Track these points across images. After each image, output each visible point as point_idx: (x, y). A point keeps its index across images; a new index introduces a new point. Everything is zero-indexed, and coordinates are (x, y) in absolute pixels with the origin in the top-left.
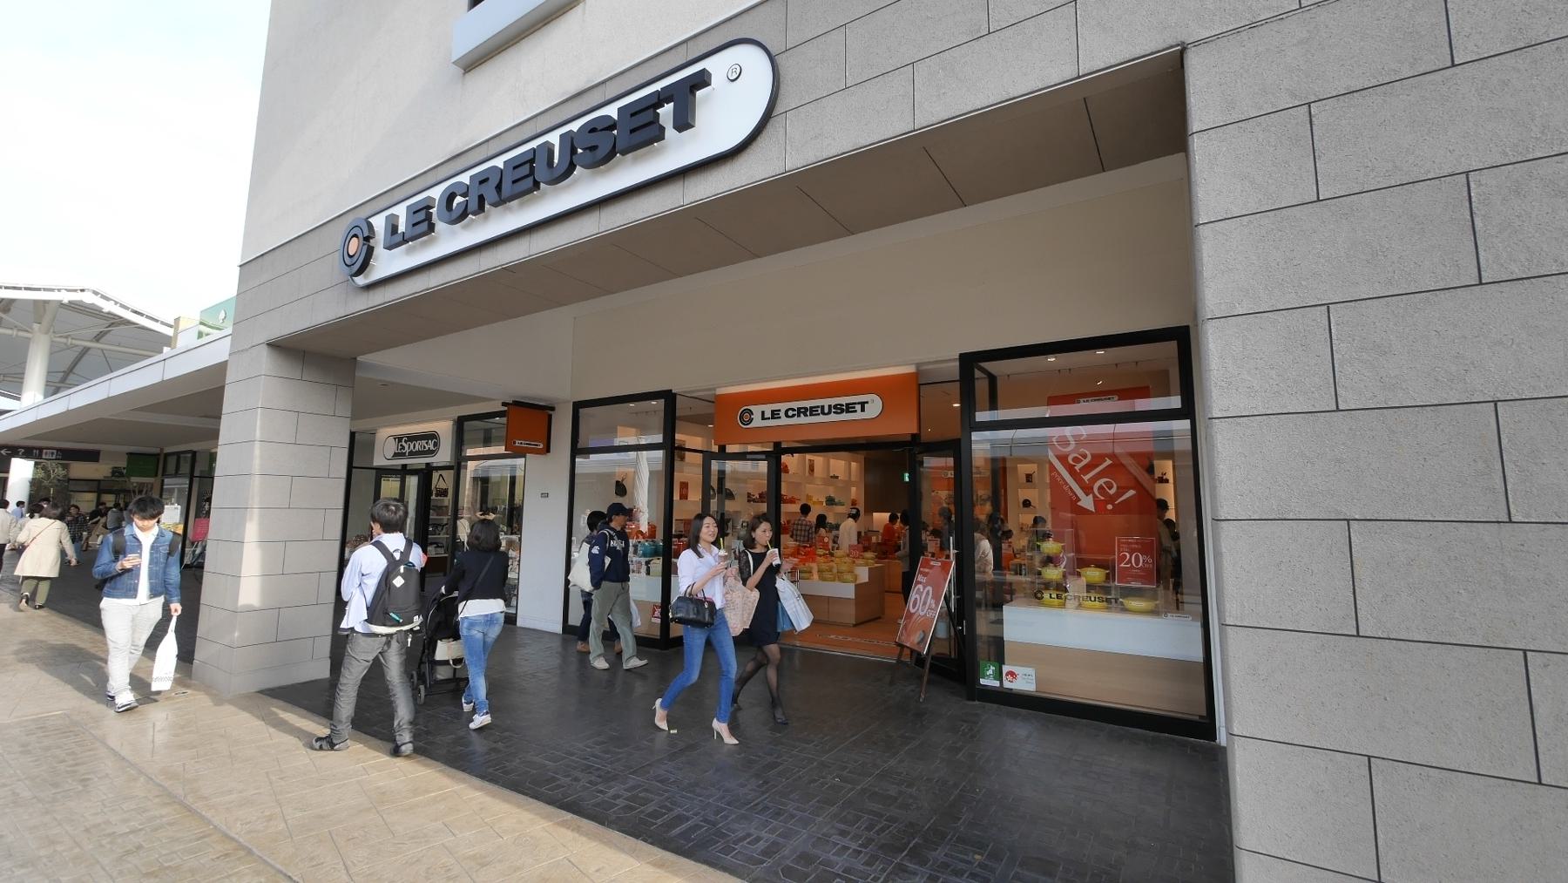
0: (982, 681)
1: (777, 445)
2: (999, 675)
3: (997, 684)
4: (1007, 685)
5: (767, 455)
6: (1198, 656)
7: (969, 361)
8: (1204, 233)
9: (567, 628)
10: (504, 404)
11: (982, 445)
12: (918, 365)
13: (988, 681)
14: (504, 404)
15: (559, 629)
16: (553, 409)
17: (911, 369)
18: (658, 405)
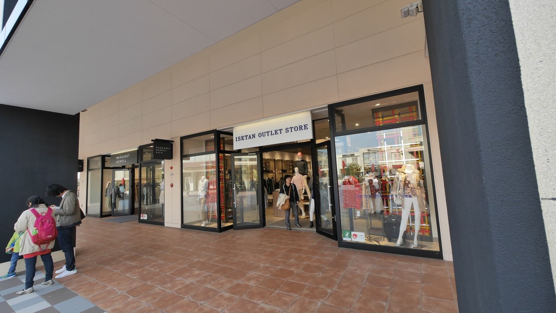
0: (344, 239)
5: (257, 153)
9: (184, 226)
10: (152, 140)
11: (339, 142)
13: (346, 239)
14: (152, 140)
15: (179, 226)
16: (173, 141)
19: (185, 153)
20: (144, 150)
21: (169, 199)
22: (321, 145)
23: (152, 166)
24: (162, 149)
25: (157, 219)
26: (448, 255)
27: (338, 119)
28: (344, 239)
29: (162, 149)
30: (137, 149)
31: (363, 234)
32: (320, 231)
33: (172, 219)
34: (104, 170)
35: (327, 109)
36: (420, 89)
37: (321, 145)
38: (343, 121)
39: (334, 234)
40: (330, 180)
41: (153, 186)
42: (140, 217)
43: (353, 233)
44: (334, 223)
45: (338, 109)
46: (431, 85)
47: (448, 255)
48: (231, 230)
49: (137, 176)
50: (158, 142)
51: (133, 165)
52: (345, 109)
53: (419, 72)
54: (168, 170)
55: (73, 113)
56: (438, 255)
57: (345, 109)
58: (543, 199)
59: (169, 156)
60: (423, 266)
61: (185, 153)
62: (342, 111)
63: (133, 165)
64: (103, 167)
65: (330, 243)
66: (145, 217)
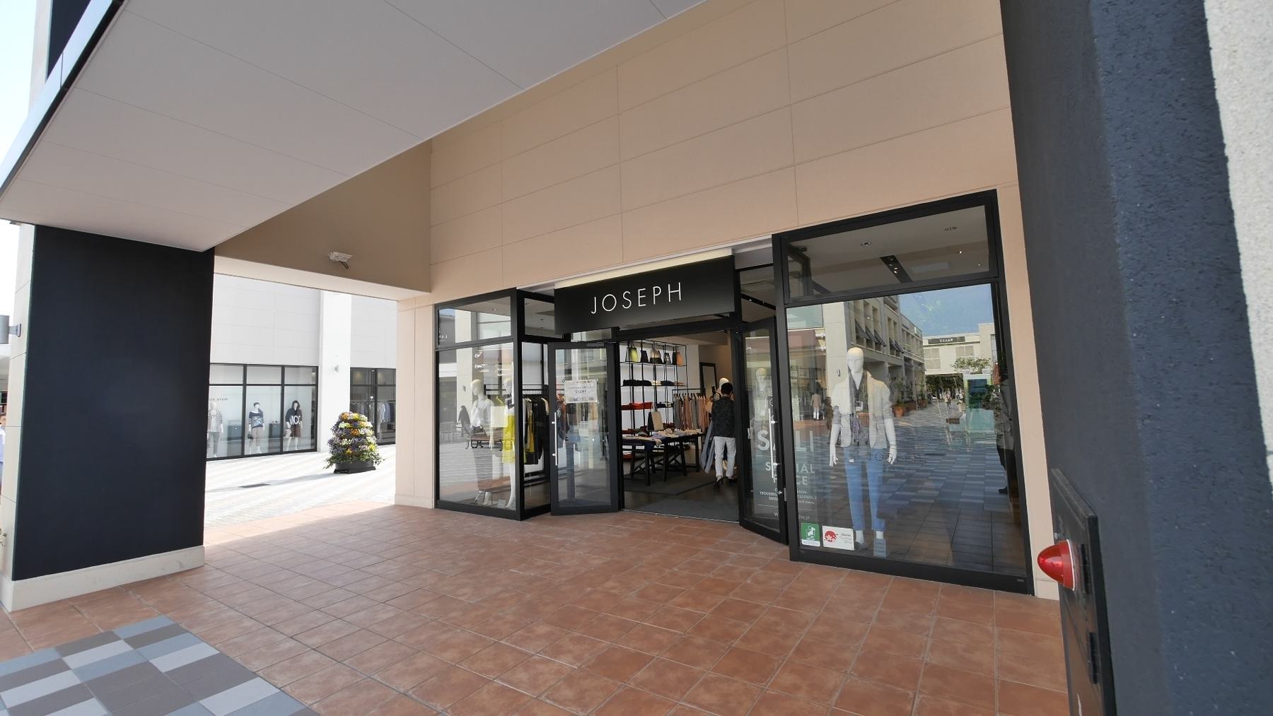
0: (804, 542)
3: (817, 544)
4: (827, 544)
5: (604, 343)
7: (786, 244)
11: (796, 320)
15: (429, 503)
17: (728, 253)
28: (804, 542)
35: (771, 245)
36: (988, 200)
37: (756, 326)
38: (806, 272)
39: (783, 530)
43: (826, 529)
44: (783, 505)
48: (548, 516)
52: (814, 246)
57: (814, 246)
62: (805, 249)
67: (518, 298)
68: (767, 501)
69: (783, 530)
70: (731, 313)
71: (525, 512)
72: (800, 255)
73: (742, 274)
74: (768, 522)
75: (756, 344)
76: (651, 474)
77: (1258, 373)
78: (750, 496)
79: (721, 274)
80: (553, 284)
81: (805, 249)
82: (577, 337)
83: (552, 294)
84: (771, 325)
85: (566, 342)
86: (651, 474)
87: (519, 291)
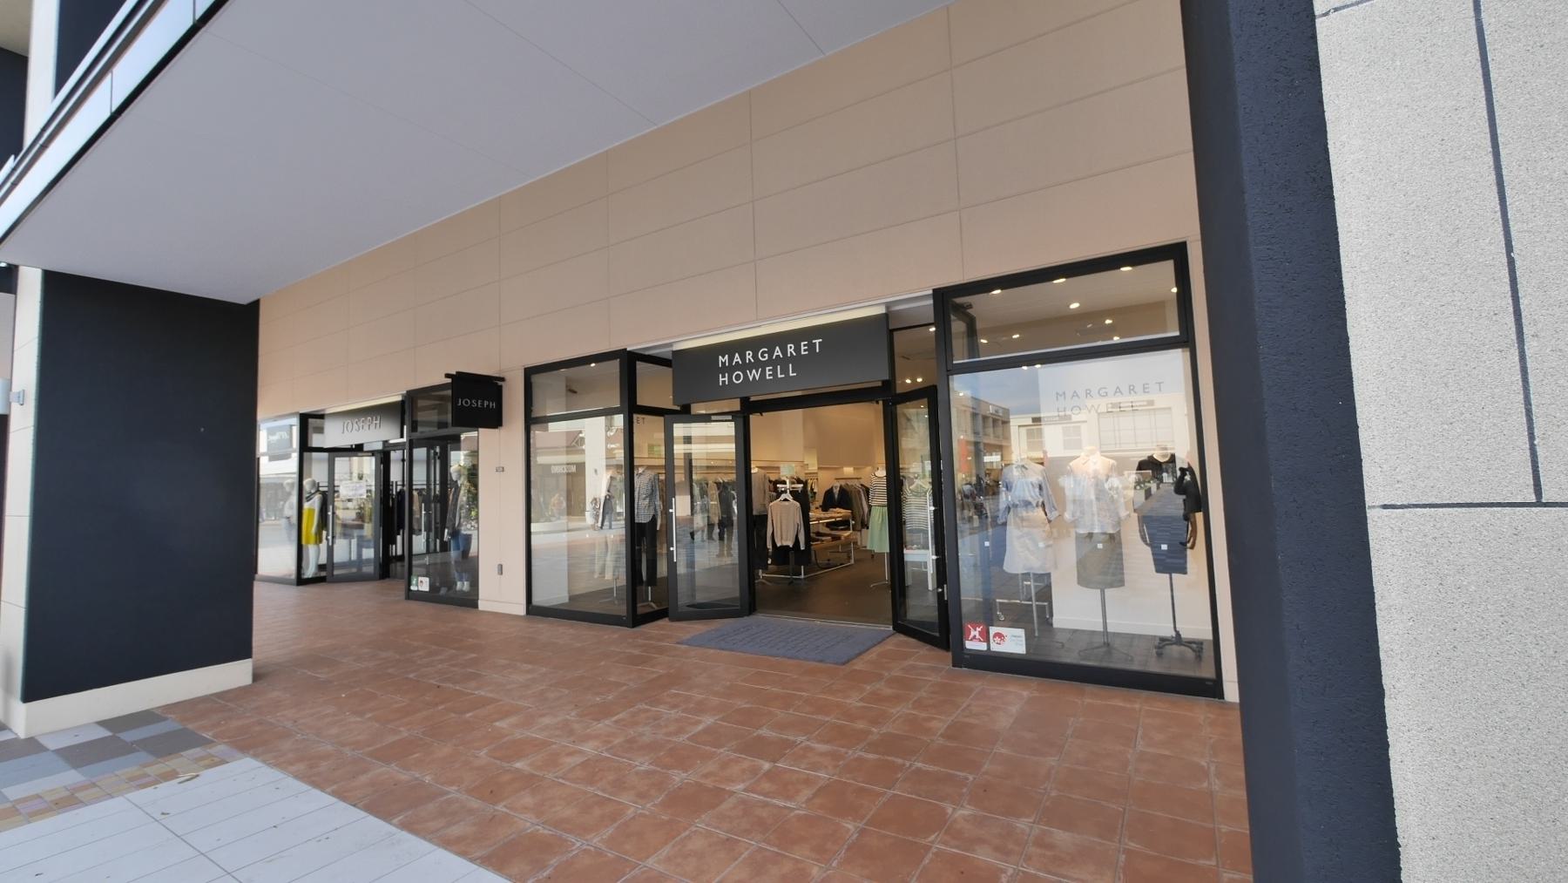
0: (969, 645)
1: (745, 401)
2: (1019, 538)
3: (983, 647)
4: (995, 647)
5: (734, 415)
6: (1208, 635)
7: (947, 301)
8: (1321, 25)
9: (532, 610)
10: (448, 376)
11: (962, 389)
12: (888, 305)
13: (974, 644)
14: (448, 376)
15: (521, 610)
16: (503, 379)
17: (881, 310)
18: (614, 367)
19: (537, 412)
20: (421, 403)
21: (495, 534)
22: (913, 396)
23: (443, 444)
24: (474, 401)
25: (455, 590)
26: (1232, 692)
27: (958, 326)
28: (969, 645)
29: (474, 401)
30: (399, 398)
31: (1021, 632)
32: (903, 627)
33: (500, 592)
34: (306, 454)
35: (931, 302)
36: (1176, 253)
37: (913, 396)
38: (972, 332)
39: (942, 632)
40: (933, 483)
41: (442, 501)
42: (409, 584)
43: (993, 630)
44: (943, 605)
45: (959, 300)
46: (1199, 244)
47: (1232, 692)
48: (664, 622)
49: (396, 475)
50: (462, 382)
51: (385, 442)
52: (980, 304)
53: (1185, 226)
54: (493, 453)
55: (243, 298)
56: (1212, 689)
57: (980, 304)
58: (911, 531)
59: (494, 419)
60: (1199, 709)
61: (536, 413)
62: (970, 306)
63: (385, 442)
64: (305, 447)
65: (926, 661)
66: (422, 584)
67: (629, 361)
68: (922, 606)
69: (942, 632)
70: (884, 382)
71: (637, 619)
72: (962, 311)
73: (538, 600)
74: (922, 624)
75: (915, 421)
76: (788, 570)
77: (1357, 398)
78: (904, 603)
79: (886, 328)
80: (671, 345)
81: (970, 306)
82: (699, 409)
83: (670, 357)
84: (933, 398)
85: (684, 413)
86: (788, 570)
87: (630, 352)
